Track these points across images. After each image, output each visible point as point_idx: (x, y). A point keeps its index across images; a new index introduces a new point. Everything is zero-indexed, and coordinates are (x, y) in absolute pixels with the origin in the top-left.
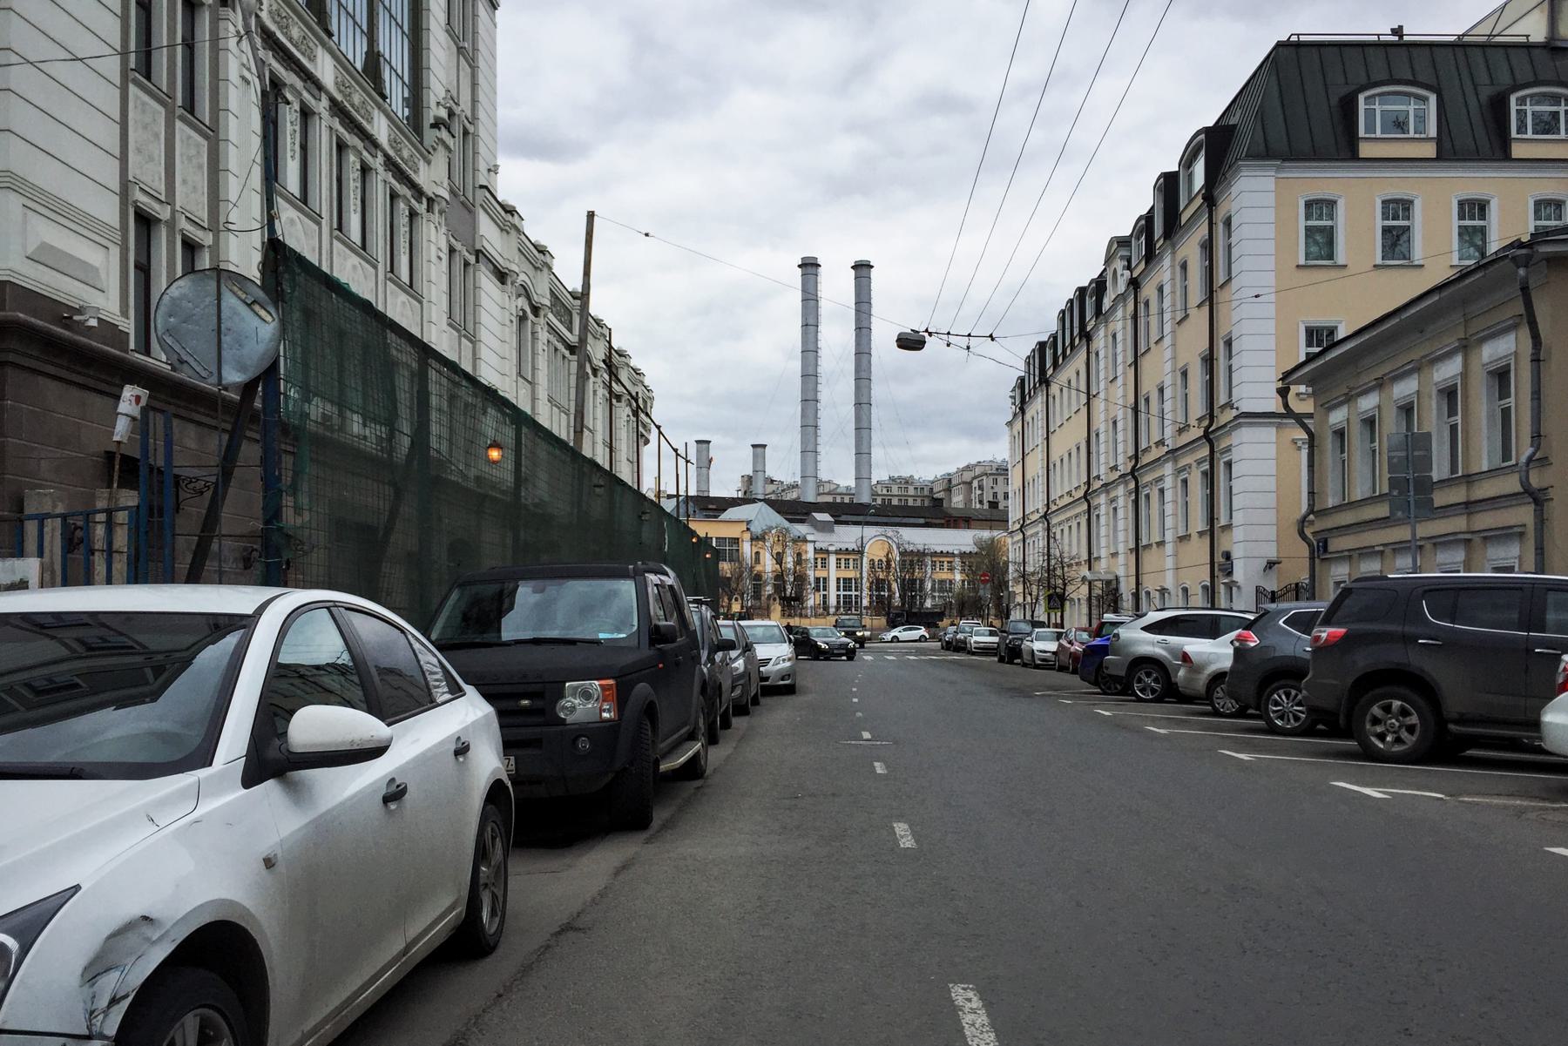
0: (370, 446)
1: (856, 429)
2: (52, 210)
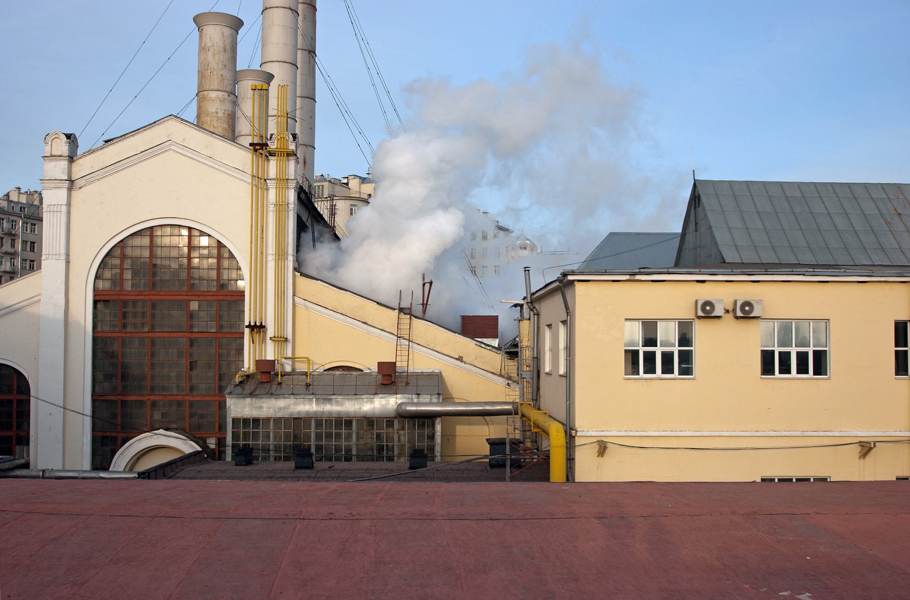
0: (120, 248)
1: (156, 479)
2: (569, 394)
